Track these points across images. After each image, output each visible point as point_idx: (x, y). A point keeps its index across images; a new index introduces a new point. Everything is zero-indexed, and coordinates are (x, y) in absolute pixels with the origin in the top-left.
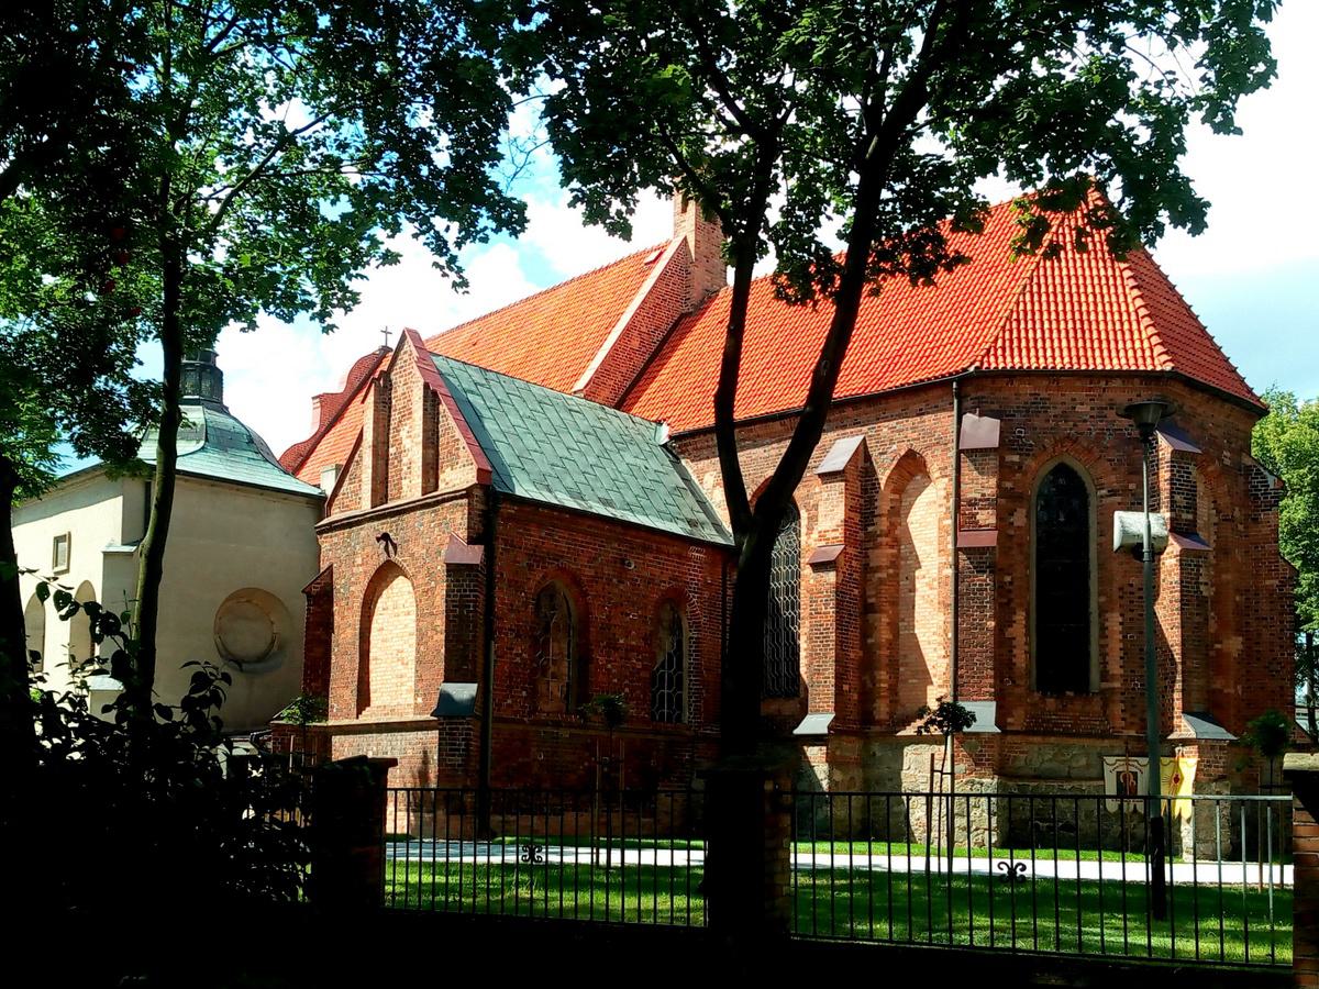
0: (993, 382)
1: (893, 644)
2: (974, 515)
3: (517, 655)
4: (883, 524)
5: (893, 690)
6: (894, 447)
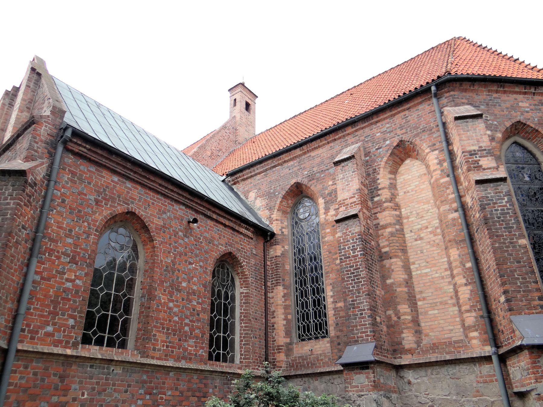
0: (461, 85)
1: (409, 282)
2: (477, 162)
3: (68, 280)
4: (385, 194)
5: (416, 321)
6: (388, 142)
